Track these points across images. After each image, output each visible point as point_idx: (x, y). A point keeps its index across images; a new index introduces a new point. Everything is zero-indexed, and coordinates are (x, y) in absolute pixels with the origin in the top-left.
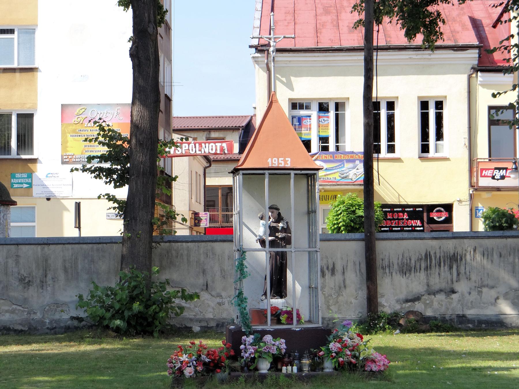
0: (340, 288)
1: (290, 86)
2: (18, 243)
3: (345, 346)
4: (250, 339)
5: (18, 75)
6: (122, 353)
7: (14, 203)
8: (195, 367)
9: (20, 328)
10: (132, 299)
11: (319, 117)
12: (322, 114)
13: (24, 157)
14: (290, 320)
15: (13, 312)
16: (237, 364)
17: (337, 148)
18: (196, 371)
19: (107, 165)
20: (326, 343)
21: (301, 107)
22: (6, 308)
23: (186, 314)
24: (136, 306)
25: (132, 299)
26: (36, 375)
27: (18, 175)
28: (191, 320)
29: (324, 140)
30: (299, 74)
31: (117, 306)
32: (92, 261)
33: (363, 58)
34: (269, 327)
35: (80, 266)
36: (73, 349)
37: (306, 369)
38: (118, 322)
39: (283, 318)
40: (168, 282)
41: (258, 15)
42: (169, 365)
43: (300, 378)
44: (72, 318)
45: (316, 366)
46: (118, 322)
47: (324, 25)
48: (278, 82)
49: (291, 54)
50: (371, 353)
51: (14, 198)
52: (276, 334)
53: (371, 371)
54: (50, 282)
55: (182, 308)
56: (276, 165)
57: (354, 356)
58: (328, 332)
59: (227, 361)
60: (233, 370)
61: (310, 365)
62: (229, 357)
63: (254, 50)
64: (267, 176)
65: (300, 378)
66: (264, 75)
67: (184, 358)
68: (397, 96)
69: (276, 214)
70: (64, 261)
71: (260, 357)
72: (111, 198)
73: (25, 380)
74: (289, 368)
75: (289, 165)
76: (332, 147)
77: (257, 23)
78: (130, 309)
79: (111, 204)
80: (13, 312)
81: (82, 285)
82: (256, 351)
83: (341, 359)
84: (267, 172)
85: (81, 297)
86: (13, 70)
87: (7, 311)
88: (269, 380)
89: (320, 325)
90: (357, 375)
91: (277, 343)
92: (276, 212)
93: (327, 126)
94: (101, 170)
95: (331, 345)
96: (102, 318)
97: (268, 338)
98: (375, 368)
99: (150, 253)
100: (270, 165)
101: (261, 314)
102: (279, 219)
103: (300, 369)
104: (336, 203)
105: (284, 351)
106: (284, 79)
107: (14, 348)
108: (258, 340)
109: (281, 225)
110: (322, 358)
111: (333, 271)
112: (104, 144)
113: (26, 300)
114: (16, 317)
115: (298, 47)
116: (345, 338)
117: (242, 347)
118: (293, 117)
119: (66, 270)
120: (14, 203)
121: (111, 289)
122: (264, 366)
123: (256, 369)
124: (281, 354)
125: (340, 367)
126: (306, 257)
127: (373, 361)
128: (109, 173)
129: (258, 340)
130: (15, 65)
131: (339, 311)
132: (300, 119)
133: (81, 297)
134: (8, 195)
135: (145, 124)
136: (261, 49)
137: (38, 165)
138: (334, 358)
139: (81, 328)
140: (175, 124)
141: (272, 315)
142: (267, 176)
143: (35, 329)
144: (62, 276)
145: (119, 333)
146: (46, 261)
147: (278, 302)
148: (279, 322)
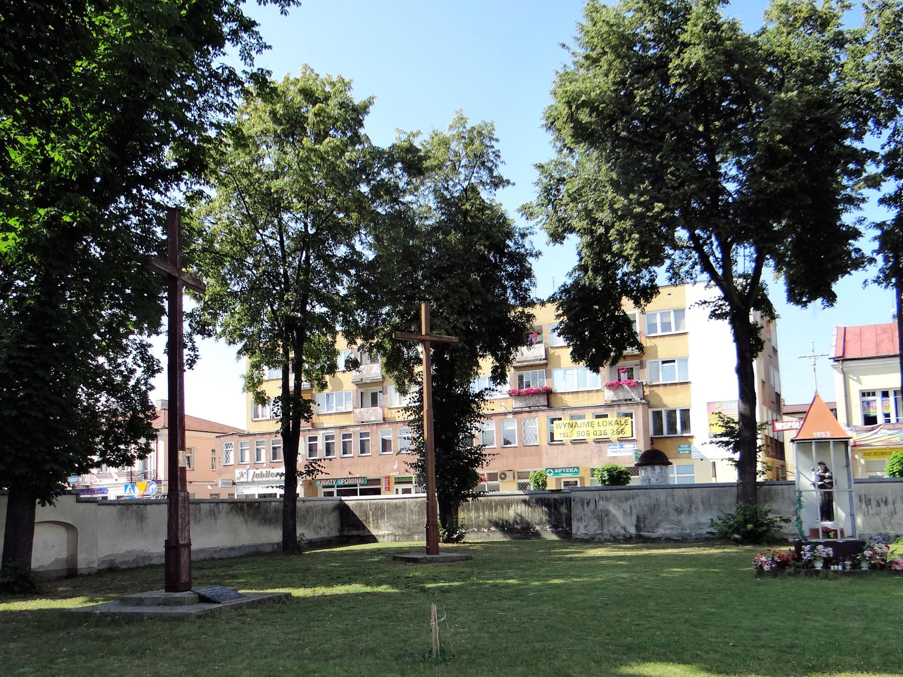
0: (892, 514)
1: (859, 381)
2: (674, 487)
3: (876, 554)
4: (807, 548)
5: (678, 386)
6: (734, 555)
7: (671, 464)
8: (771, 565)
9: (677, 538)
10: (746, 522)
11: (882, 401)
12: (884, 399)
13: (685, 435)
14: (836, 536)
15: (672, 529)
16: (800, 563)
17: (897, 420)
18: (771, 567)
19: (726, 439)
20: (862, 551)
21: (869, 394)
22: (668, 526)
23: (782, 530)
24: (750, 526)
25: (746, 522)
26: (675, 567)
27: (682, 446)
28: (787, 534)
29: (887, 415)
30: (866, 374)
31: (736, 525)
32: (720, 497)
33: (899, 361)
34: (821, 540)
35: (712, 501)
36: (705, 552)
37: (848, 568)
38: (736, 536)
39: (831, 534)
40: (770, 511)
41: (835, 338)
42: (753, 563)
43: (844, 573)
44: (708, 533)
45: (856, 565)
46: (736, 536)
47: (882, 341)
48: (850, 380)
49: (859, 361)
50: (896, 557)
51: (670, 461)
52: (826, 545)
53: (896, 570)
54: (694, 511)
55: (781, 527)
56: (819, 437)
57: (883, 560)
58: (863, 543)
59: (792, 562)
60: (798, 567)
61: (851, 565)
62: (794, 559)
63: (832, 360)
64: (813, 443)
65: (844, 573)
66: (841, 376)
67: (763, 559)
68: (706, 404)
69: (823, 468)
70: (702, 498)
71: (814, 559)
72: (730, 459)
73: (666, 570)
74: (836, 567)
75: (828, 436)
76: (893, 419)
77: (834, 343)
78: (745, 527)
79: (730, 462)
80: (672, 529)
81: (715, 513)
82: (812, 555)
83: (873, 562)
84: (813, 441)
85: (712, 520)
86: (676, 384)
87: (669, 528)
88: (821, 574)
89: (857, 539)
90: (885, 572)
91: (826, 550)
92: (823, 466)
93: (888, 406)
94: (722, 442)
95: (865, 552)
96: (726, 533)
97: (820, 547)
98: (898, 568)
99: (756, 492)
100: (815, 437)
101: (814, 532)
102: (826, 470)
103: (844, 568)
104: (891, 458)
105: (831, 555)
106: (855, 378)
107: (669, 551)
108: (813, 549)
109: (827, 474)
110: (860, 561)
111: (886, 503)
112: (722, 426)
113: (679, 522)
114: (674, 532)
115: (863, 356)
116: (876, 548)
117: (802, 552)
118: (863, 402)
119: (703, 503)
120: (671, 464)
121: (731, 515)
122: (819, 565)
123: (813, 567)
124: (829, 557)
125: (873, 567)
126: (847, 495)
127: (897, 563)
128: (727, 444)
129: (813, 549)
130: (677, 381)
131: (892, 529)
132: (868, 403)
133: (712, 520)
134: (667, 459)
135: (748, 413)
136: (841, 359)
137: (694, 440)
138: (868, 561)
139: (715, 539)
140: (784, 410)
141: (823, 532)
142: (813, 443)
143: (686, 539)
144: (701, 507)
145: (737, 542)
146: (691, 498)
147: (828, 524)
148: (829, 537)
